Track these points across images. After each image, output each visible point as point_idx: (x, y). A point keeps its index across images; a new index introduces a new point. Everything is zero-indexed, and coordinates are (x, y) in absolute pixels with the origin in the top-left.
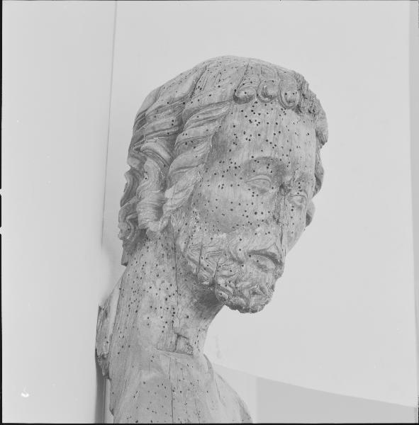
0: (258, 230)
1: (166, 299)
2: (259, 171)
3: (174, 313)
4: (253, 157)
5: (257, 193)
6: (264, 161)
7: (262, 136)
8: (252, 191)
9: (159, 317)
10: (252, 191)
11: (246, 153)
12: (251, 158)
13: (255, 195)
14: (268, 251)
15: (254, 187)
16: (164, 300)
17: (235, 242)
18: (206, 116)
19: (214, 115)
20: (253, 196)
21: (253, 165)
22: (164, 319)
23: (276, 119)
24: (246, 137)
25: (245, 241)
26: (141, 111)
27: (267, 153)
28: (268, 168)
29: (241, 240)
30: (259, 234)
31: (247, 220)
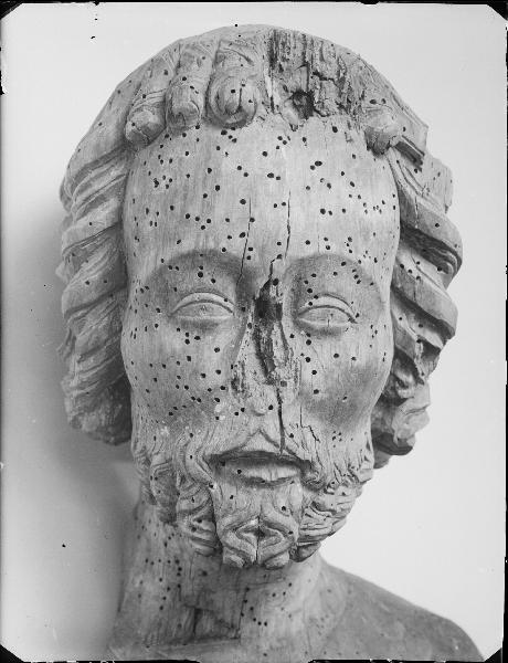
0: (218, 408)
1: (166, 545)
2: (182, 287)
3: (180, 569)
4: (162, 260)
5: (196, 334)
6: (188, 262)
7: (177, 210)
8: (183, 333)
9: (157, 580)
10: (183, 333)
11: (153, 254)
12: (159, 262)
13: (191, 339)
14: (246, 448)
15: (184, 323)
16: (163, 545)
17: (182, 443)
18: (85, 195)
19: (96, 186)
20: (187, 342)
21: (169, 276)
22: (164, 584)
23: (207, 160)
24: (150, 219)
25: (198, 440)
26: (75, 170)
27: (188, 245)
28: (201, 275)
29: (191, 435)
30: (222, 418)
31: (188, 394)
